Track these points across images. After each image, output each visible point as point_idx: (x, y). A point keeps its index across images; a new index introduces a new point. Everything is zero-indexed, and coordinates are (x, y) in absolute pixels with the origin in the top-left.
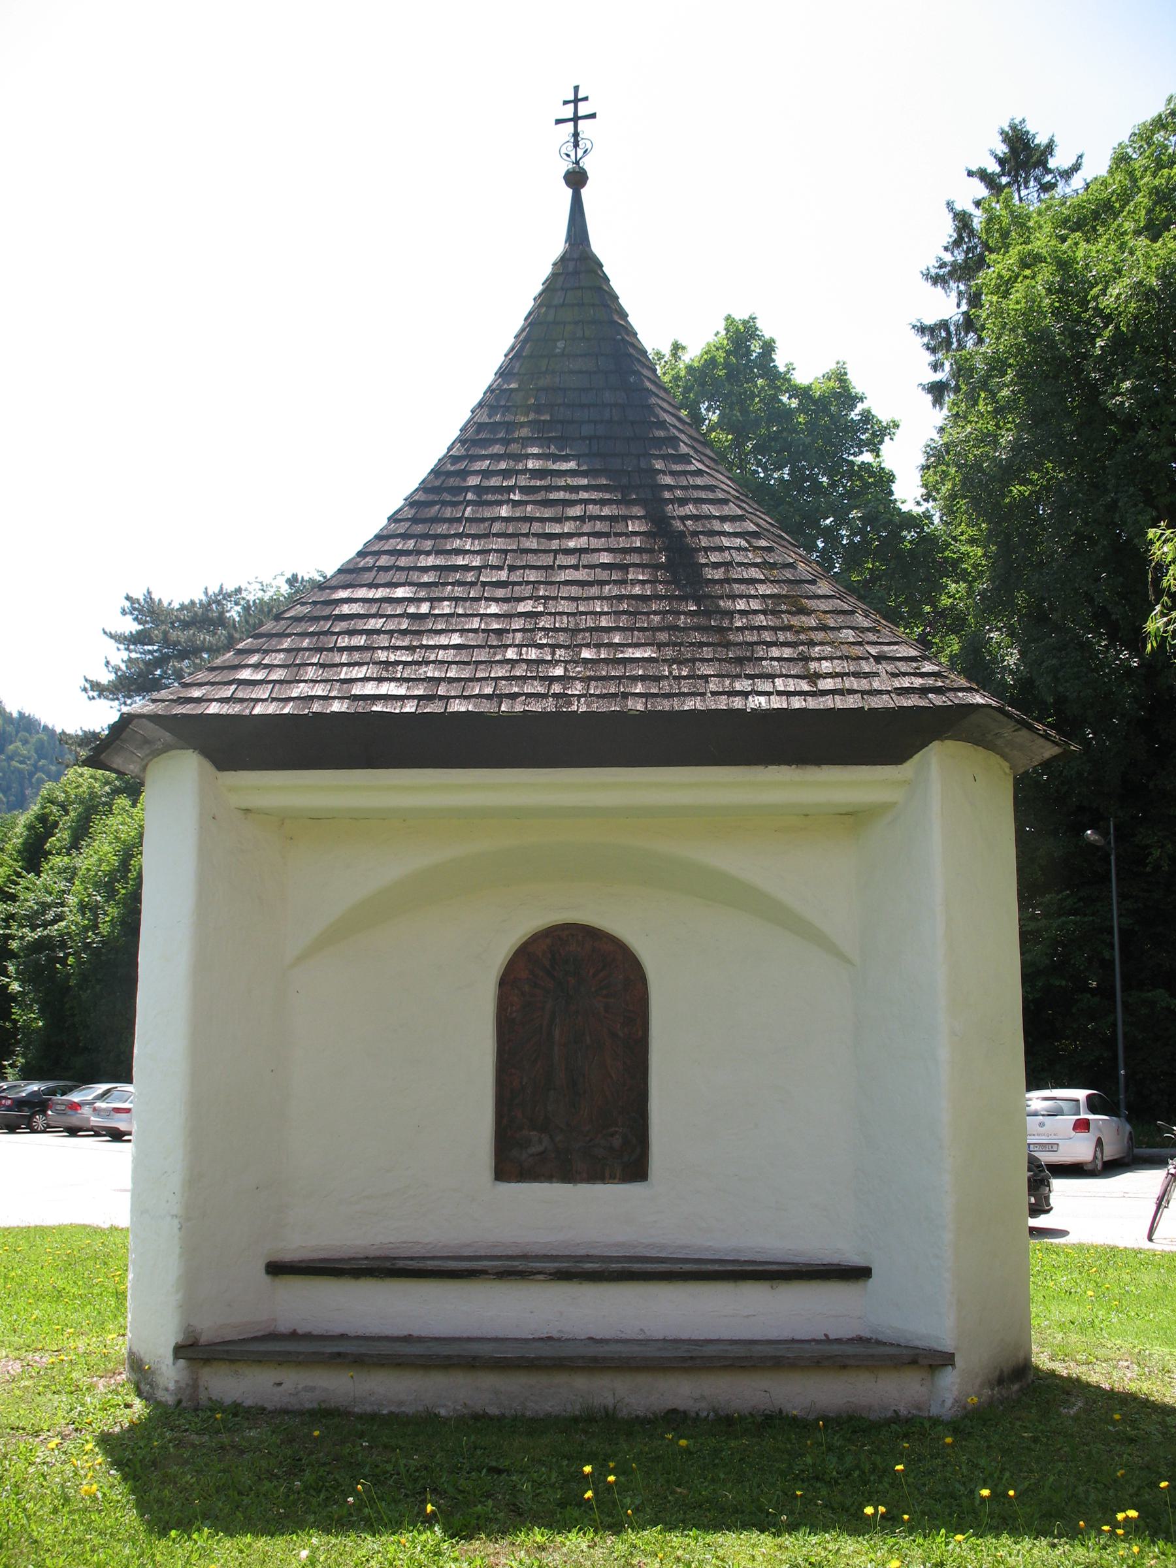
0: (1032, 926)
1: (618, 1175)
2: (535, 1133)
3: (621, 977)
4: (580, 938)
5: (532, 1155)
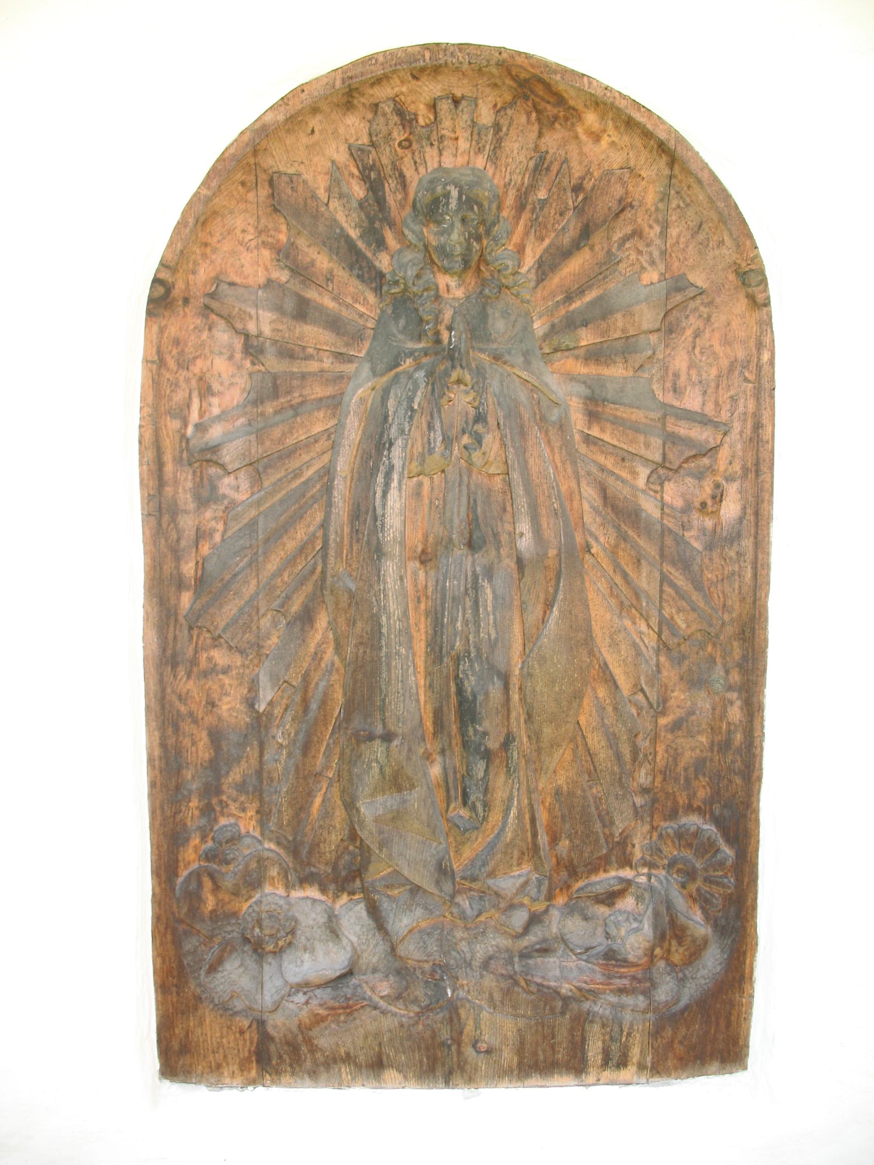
0: (761, 287)
1: (635, 1053)
2: (313, 892)
3: (652, 276)
4: (486, 116)
5: (305, 986)
